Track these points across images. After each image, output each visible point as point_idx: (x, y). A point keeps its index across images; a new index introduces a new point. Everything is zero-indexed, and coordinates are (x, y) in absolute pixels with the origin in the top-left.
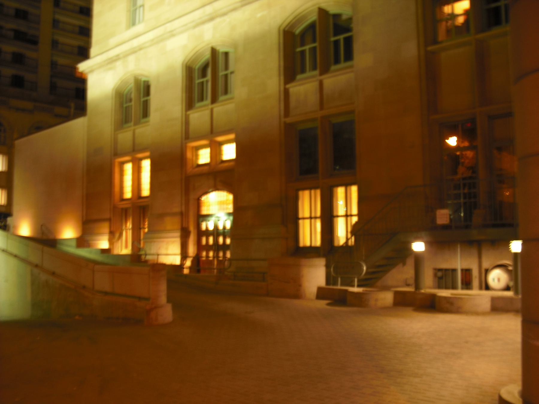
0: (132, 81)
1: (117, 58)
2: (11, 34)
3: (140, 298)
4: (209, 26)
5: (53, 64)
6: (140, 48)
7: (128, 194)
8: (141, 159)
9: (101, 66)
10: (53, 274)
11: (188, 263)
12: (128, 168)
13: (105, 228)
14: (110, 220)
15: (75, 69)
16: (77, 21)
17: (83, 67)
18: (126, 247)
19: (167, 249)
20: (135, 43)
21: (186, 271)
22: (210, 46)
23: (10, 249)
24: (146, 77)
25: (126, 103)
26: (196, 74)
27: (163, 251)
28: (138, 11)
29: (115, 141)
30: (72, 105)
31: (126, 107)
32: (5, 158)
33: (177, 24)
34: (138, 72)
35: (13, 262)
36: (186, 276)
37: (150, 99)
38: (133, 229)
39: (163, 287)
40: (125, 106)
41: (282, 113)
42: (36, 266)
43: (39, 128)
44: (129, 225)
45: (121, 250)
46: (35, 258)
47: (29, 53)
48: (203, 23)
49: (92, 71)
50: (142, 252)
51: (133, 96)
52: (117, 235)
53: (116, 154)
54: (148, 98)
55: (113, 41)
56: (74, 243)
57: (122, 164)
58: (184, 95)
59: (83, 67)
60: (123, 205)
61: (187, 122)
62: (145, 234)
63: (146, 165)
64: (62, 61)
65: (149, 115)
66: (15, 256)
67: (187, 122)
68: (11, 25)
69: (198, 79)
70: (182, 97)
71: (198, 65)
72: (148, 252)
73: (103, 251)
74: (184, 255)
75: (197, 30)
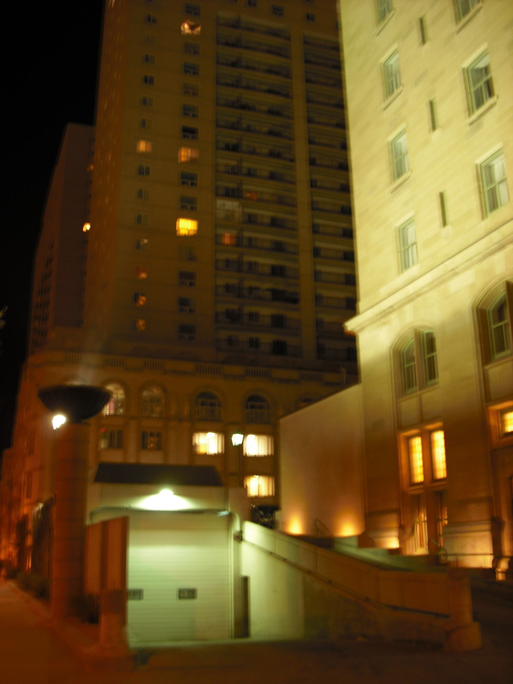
0: (411, 335)
1: (391, 310)
2: (268, 295)
3: (438, 615)
4: (499, 257)
5: (319, 323)
6: (418, 295)
7: (419, 477)
8: (431, 432)
9: (373, 321)
10: (330, 582)
11: (504, 565)
12: (417, 443)
13: (393, 521)
14: (398, 511)
15: (342, 329)
16: (342, 270)
17: (351, 325)
18: (421, 545)
19: (474, 546)
20: (411, 289)
21: (500, 577)
22: (504, 280)
23: (277, 552)
24: (430, 328)
25: (408, 363)
26: (491, 318)
27: (469, 550)
28: (410, 250)
29: (398, 411)
30: (344, 370)
31: (408, 368)
32: (270, 439)
33: (459, 259)
34: (418, 323)
35: (282, 567)
36: (501, 583)
37: (436, 355)
38: (428, 522)
39: (467, 600)
40: (406, 366)
41: (484, 397)
42: (309, 572)
43: (309, 400)
44: (423, 516)
45: (416, 551)
46: (307, 564)
47: (290, 313)
48: (492, 253)
49: (362, 329)
50: (441, 552)
51: (415, 354)
52: (409, 530)
53: (401, 427)
54: (434, 354)
55: (384, 291)
56: (354, 542)
57: (409, 439)
58: (479, 346)
59: (351, 325)
60: (413, 491)
61: (485, 380)
62: (445, 527)
63: (439, 438)
64: (328, 318)
65: (438, 377)
66: (285, 560)
67: (485, 380)
68: (267, 285)
69: (495, 323)
70: (477, 348)
71: (491, 307)
72: (449, 552)
73: (392, 552)
74: (498, 555)
75: (485, 263)
